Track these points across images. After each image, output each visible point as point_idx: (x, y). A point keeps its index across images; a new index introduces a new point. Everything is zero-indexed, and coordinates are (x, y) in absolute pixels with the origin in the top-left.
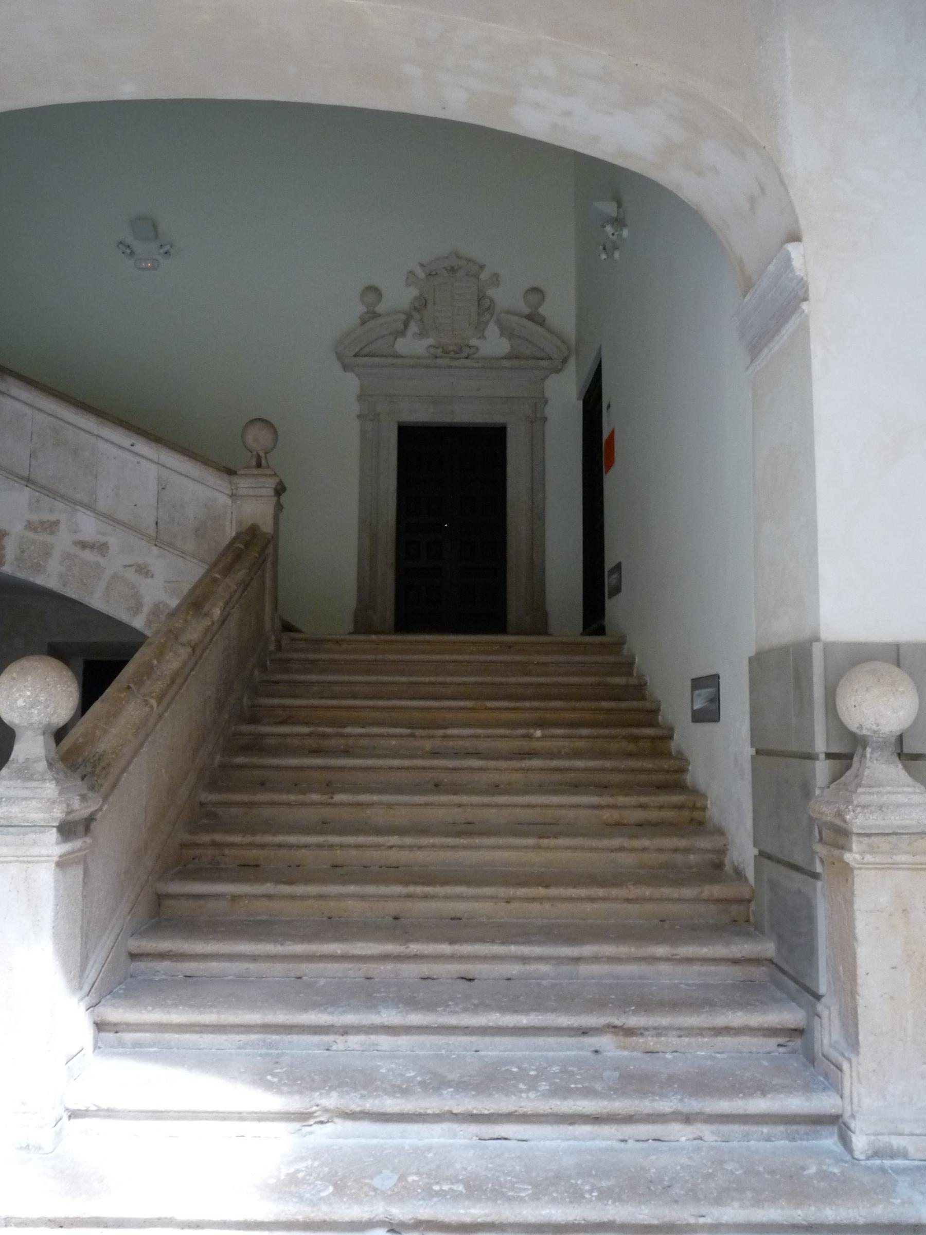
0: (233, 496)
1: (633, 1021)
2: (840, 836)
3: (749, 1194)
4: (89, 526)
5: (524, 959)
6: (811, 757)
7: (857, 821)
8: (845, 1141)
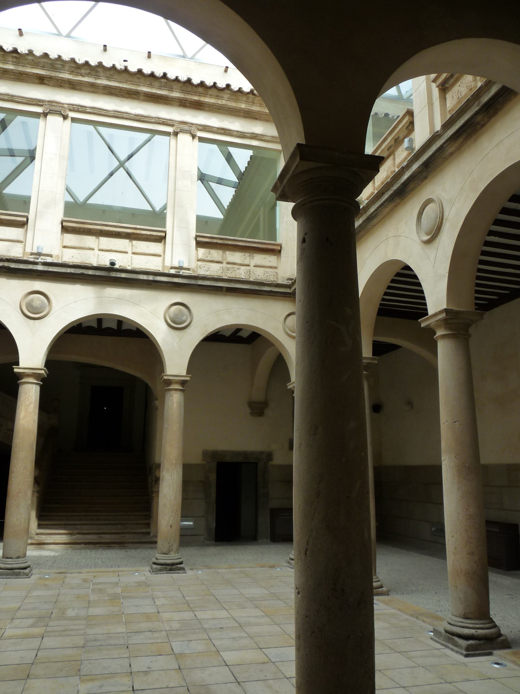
1: (124, 522)
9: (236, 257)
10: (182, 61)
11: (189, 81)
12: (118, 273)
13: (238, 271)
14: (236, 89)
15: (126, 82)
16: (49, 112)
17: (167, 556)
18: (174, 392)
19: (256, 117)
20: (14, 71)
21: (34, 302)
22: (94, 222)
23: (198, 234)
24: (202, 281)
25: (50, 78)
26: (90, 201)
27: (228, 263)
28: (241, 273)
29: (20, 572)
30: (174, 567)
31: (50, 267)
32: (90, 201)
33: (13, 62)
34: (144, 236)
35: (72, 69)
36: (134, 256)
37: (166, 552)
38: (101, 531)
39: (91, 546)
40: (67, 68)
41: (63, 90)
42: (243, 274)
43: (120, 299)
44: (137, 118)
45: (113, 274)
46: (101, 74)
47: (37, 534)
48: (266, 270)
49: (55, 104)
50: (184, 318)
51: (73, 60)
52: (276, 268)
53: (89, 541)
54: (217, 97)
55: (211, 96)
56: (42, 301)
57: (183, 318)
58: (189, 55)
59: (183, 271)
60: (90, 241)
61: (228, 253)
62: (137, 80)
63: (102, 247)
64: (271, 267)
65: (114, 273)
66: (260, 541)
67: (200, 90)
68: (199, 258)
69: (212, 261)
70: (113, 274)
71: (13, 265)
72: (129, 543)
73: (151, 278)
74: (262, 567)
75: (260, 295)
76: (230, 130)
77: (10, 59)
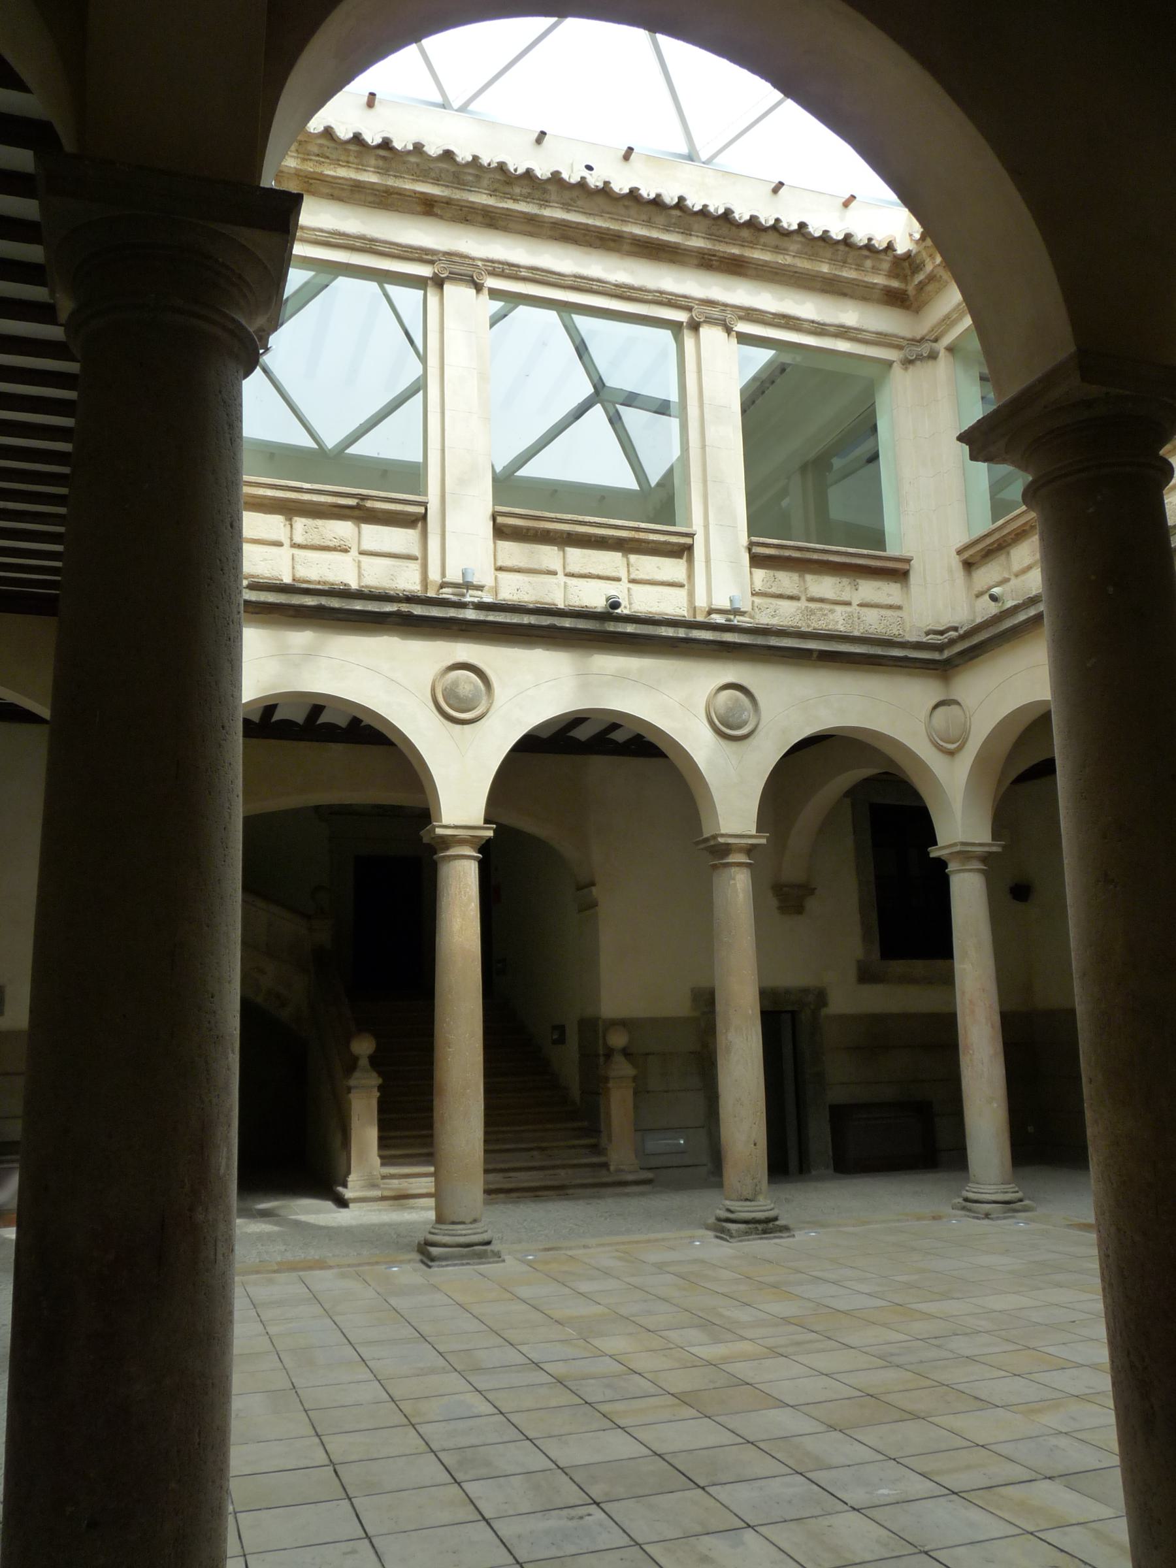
1: (544, 1145)
2: (606, 1079)
8: (608, 1170)
9: (825, 586)
10: (688, 167)
11: (727, 214)
12: (620, 624)
13: (831, 617)
14: (818, 234)
15: (600, 214)
16: (447, 278)
18: (737, 869)
19: (845, 291)
20: (376, 187)
22: (559, 516)
23: (754, 539)
25: (447, 203)
26: (352, 450)
27: (811, 599)
28: (837, 620)
29: (486, 1251)
30: (771, 1225)
32: (352, 450)
33: (378, 168)
35: (496, 186)
36: (633, 586)
39: (502, 1196)
40: (485, 183)
41: (470, 227)
42: (841, 622)
43: (621, 677)
44: (619, 291)
45: (611, 627)
46: (553, 197)
47: (384, 1177)
48: (883, 612)
49: (457, 259)
51: (502, 167)
52: (899, 608)
54: (777, 249)
55: (765, 247)
58: (704, 156)
60: (548, 556)
61: (809, 578)
62: (622, 211)
63: (571, 568)
64: (890, 607)
66: (814, 1173)
67: (745, 233)
69: (780, 596)
70: (611, 627)
71: (418, 610)
73: (681, 633)
74: (919, 1219)
75: (880, 665)
76: (798, 319)
77: (373, 162)
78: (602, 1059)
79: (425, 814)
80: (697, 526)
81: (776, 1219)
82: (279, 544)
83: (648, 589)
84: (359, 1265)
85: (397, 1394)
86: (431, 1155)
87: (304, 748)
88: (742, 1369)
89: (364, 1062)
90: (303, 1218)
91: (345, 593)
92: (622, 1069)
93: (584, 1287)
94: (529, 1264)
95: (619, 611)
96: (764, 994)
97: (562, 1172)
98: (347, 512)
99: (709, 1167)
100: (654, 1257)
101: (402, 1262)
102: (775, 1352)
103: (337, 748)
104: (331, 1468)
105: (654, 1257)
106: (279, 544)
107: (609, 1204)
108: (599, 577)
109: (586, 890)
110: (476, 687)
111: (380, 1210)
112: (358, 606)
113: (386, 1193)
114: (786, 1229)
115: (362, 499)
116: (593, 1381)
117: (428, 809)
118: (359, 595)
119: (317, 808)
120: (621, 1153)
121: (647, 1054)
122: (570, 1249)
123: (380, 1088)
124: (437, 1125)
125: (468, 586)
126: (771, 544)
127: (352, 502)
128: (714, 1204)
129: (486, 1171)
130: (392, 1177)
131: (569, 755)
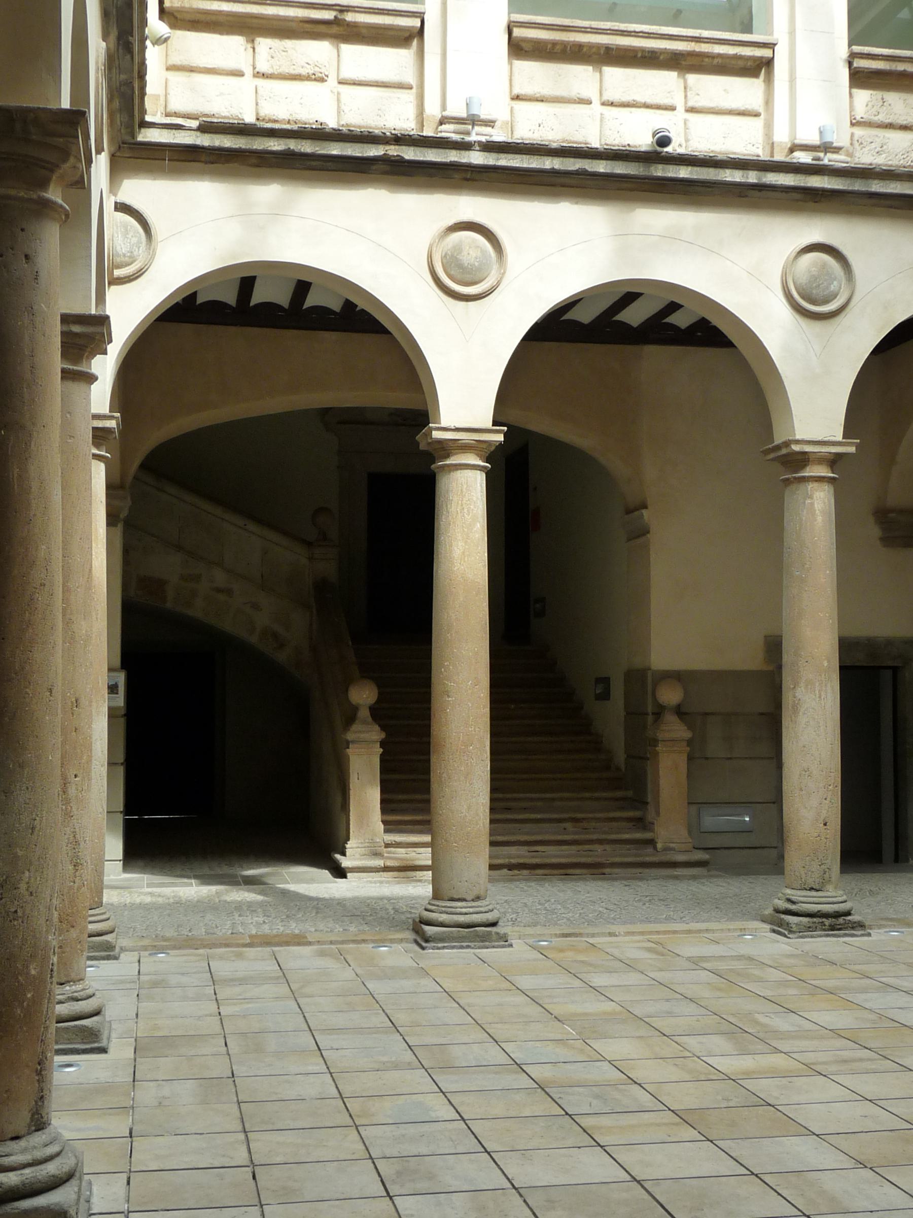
0: (311, 559)
1: (579, 816)
2: (655, 742)
3: (639, 55)
4: (220, 577)
5: (532, 800)
6: (647, 714)
7: (660, 736)
8: (655, 848)
12: (671, 167)
17: (820, 894)
18: (816, 485)
21: (465, 253)
22: (595, 24)
23: (856, 49)
24: (882, 183)
29: (490, 933)
30: (841, 920)
31: (502, 156)
34: (716, 61)
36: (690, 116)
37: (816, 887)
38: (539, 838)
39: (525, 872)
45: (659, 171)
47: (387, 845)
50: (834, 287)
53: (521, 861)
56: (482, 251)
57: (832, 288)
59: (830, 156)
60: (579, 78)
63: (609, 96)
65: (660, 166)
68: (858, 118)
69: (890, 126)
70: (659, 171)
71: (410, 154)
72: (613, 865)
73: (752, 177)
78: (650, 718)
79: (421, 416)
80: (779, 33)
81: (848, 913)
82: (239, 74)
83: (712, 120)
84: (343, 942)
85: (347, 1090)
86: (428, 822)
87: (291, 337)
88: (766, 1087)
89: (364, 713)
90: (292, 887)
91: (320, 134)
92: (675, 729)
93: (599, 980)
94: (540, 951)
95: (669, 149)
96: (846, 646)
97: (599, 848)
98: (322, 28)
99: (761, 851)
100: (691, 949)
101: (392, 941)
102: (812, 1070)
103: (330, 337)
104: (249, 1170)
105: (691, 949)
106: (239, 74)
107: (652, 887)
108: (647, 106)
109: (636, 513)
110: (483, 252)
111: (381, 882)
112: (335, 149)
113: (389, 863)
114: (861, 925)
115: (341, 11)
116: (581, 1090)
117: (427, 411)
118: (337, 136)
119: (325, 413)
120: (670, 831)
121: (706, 714)
122: (593, 935)
123: (383, 744)
124: (434, 786)
125: (473, 120)
126: (880, 55)
127: (328, 15)
128: (775, 893)
129: (492, 844)
130: (398, 845)
131: (599, 340)
